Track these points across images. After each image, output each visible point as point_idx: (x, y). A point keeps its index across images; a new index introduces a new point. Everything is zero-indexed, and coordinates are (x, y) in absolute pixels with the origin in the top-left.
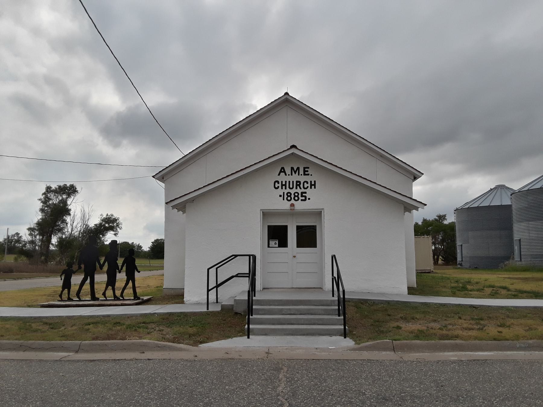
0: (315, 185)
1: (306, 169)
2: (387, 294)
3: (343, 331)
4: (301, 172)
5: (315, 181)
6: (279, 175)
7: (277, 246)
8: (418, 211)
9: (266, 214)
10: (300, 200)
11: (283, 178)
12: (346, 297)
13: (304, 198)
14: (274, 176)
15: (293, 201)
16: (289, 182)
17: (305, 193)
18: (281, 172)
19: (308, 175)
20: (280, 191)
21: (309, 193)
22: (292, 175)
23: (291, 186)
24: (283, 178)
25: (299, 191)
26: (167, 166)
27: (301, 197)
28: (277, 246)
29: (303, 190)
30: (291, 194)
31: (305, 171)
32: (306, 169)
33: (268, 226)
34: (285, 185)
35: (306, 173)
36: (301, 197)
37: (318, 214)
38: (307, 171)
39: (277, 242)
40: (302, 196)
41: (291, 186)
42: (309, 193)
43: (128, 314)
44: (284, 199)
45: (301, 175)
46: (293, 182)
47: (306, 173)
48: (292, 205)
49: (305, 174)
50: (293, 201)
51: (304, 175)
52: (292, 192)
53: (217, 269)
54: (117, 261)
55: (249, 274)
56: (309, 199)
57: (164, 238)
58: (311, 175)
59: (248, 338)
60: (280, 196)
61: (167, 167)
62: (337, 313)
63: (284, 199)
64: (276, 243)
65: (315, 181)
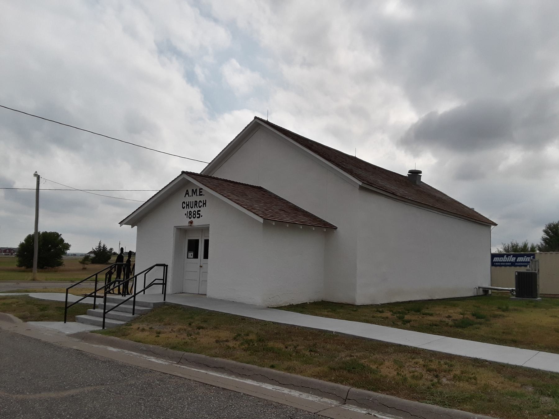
0: (205, 204)
1: (201, 190)
2: (245, 304)
3: (102, 324)
4: (198, 193)
5: (206, 200)
6: (185, 197)
7: (192, 257)
8: (132, 228)
9: (181, 231)
10: (196, 217)
11: (188, 199)
12: (96, 304)
13: (198, 216)
14: (182, 198)
15: (192, 219)
16: (191, 202)
17: (200, 211)
18: (186, 194)
19: (202, 195)
20: (186, 211)
21: (203, 211)
22: (192, 196)
23: (192, 206)
24: (188, 199)
25: (196, 210)
26: (160, 190)
27: (197, 214)
28: (192, 257)
29: (199, 209)
30: (191, 212)
31: (200, 192)
32: (201, 190)
33: (198, 240)
34: (188, 205)
35: (201, 194)
36: (197, 214)
37: (205, 229)
38: (201, 192)
39: (192, 254)
40: (198, 214)
41: (192, 206)
42: (203, 211)
43: (253, 319)
44: (187, 218)
45: (198, 195)
46: (193, 202)
47: (201, 194)
48: (191, 222)
49: (200, 195)
50: (192, 219)
51: (200, 195)
52: (192, 210)
53: (145, 274)
54: (112, 275)
55: (163, 280)
56: (202, 216)
57: (134, 250)
58: (204, 195)
59: (65, 322)
60: (185, 214)
61: (160, 191)
62: (132, 311)
63: (187, 218)
64: (192, 254)
65: (206, 200)
